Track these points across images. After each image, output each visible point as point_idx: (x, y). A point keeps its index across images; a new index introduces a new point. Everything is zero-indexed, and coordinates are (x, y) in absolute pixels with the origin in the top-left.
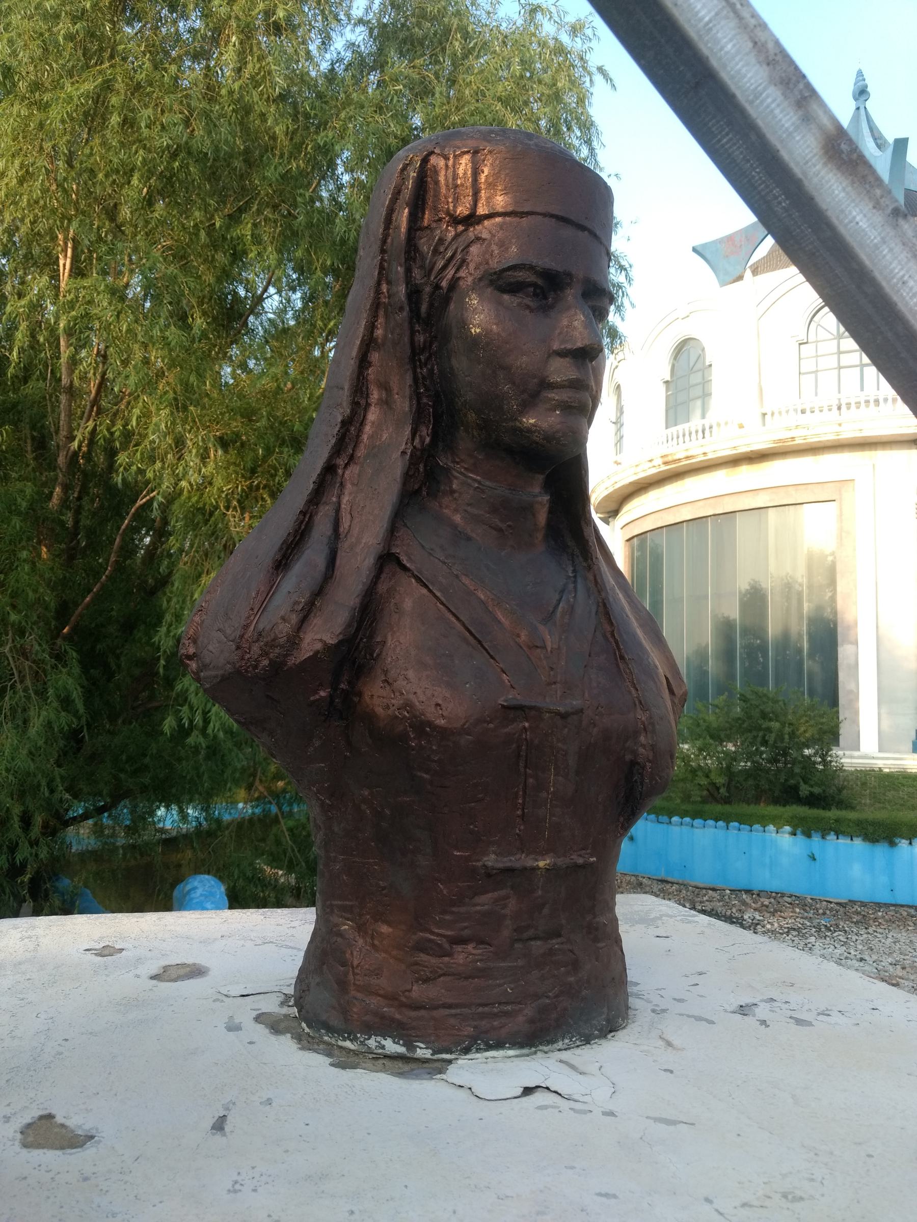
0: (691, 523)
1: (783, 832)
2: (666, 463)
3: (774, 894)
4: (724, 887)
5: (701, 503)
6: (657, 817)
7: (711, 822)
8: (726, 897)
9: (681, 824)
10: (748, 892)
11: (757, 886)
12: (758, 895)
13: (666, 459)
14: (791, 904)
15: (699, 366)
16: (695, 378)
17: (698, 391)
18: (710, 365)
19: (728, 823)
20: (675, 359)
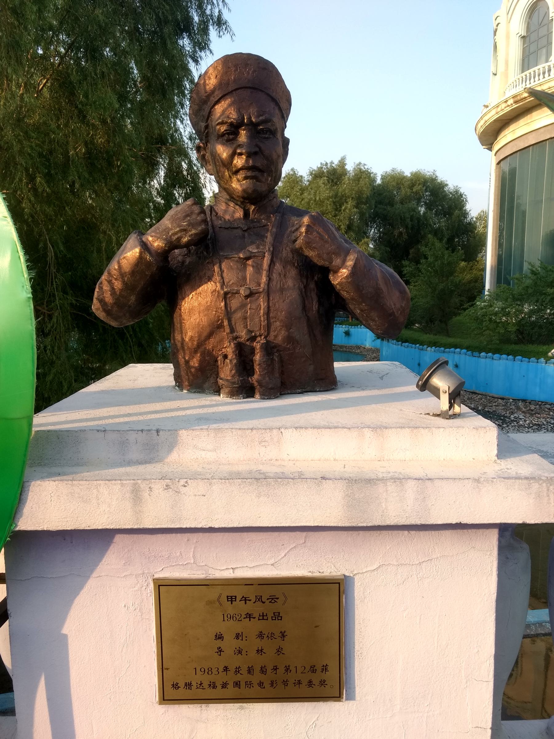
0: (535, 146)
1: (550, 363)
2: (516, 102)
3: (540, 403)
4: (510, 397)
5: (542, 130)
6: (472, 353)
7: (504, 356)
8: (509, 404)
9: (486, 357)
10: (524, 401)
11: (530, 397)
12: (530, 403)
13: (516, 99)
14: (549, 409)
15: (545, 21)
16: (543, 31)
17: (544, 41)
18: (552, 20)
19: (515, 357)
20: (529, 18)
